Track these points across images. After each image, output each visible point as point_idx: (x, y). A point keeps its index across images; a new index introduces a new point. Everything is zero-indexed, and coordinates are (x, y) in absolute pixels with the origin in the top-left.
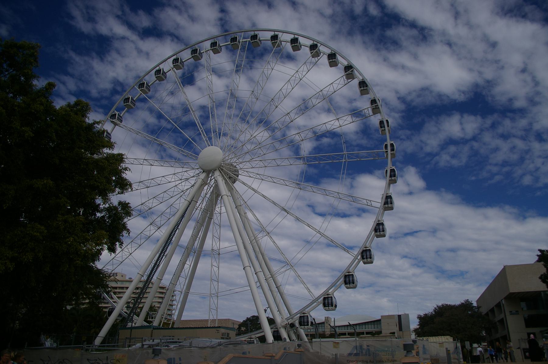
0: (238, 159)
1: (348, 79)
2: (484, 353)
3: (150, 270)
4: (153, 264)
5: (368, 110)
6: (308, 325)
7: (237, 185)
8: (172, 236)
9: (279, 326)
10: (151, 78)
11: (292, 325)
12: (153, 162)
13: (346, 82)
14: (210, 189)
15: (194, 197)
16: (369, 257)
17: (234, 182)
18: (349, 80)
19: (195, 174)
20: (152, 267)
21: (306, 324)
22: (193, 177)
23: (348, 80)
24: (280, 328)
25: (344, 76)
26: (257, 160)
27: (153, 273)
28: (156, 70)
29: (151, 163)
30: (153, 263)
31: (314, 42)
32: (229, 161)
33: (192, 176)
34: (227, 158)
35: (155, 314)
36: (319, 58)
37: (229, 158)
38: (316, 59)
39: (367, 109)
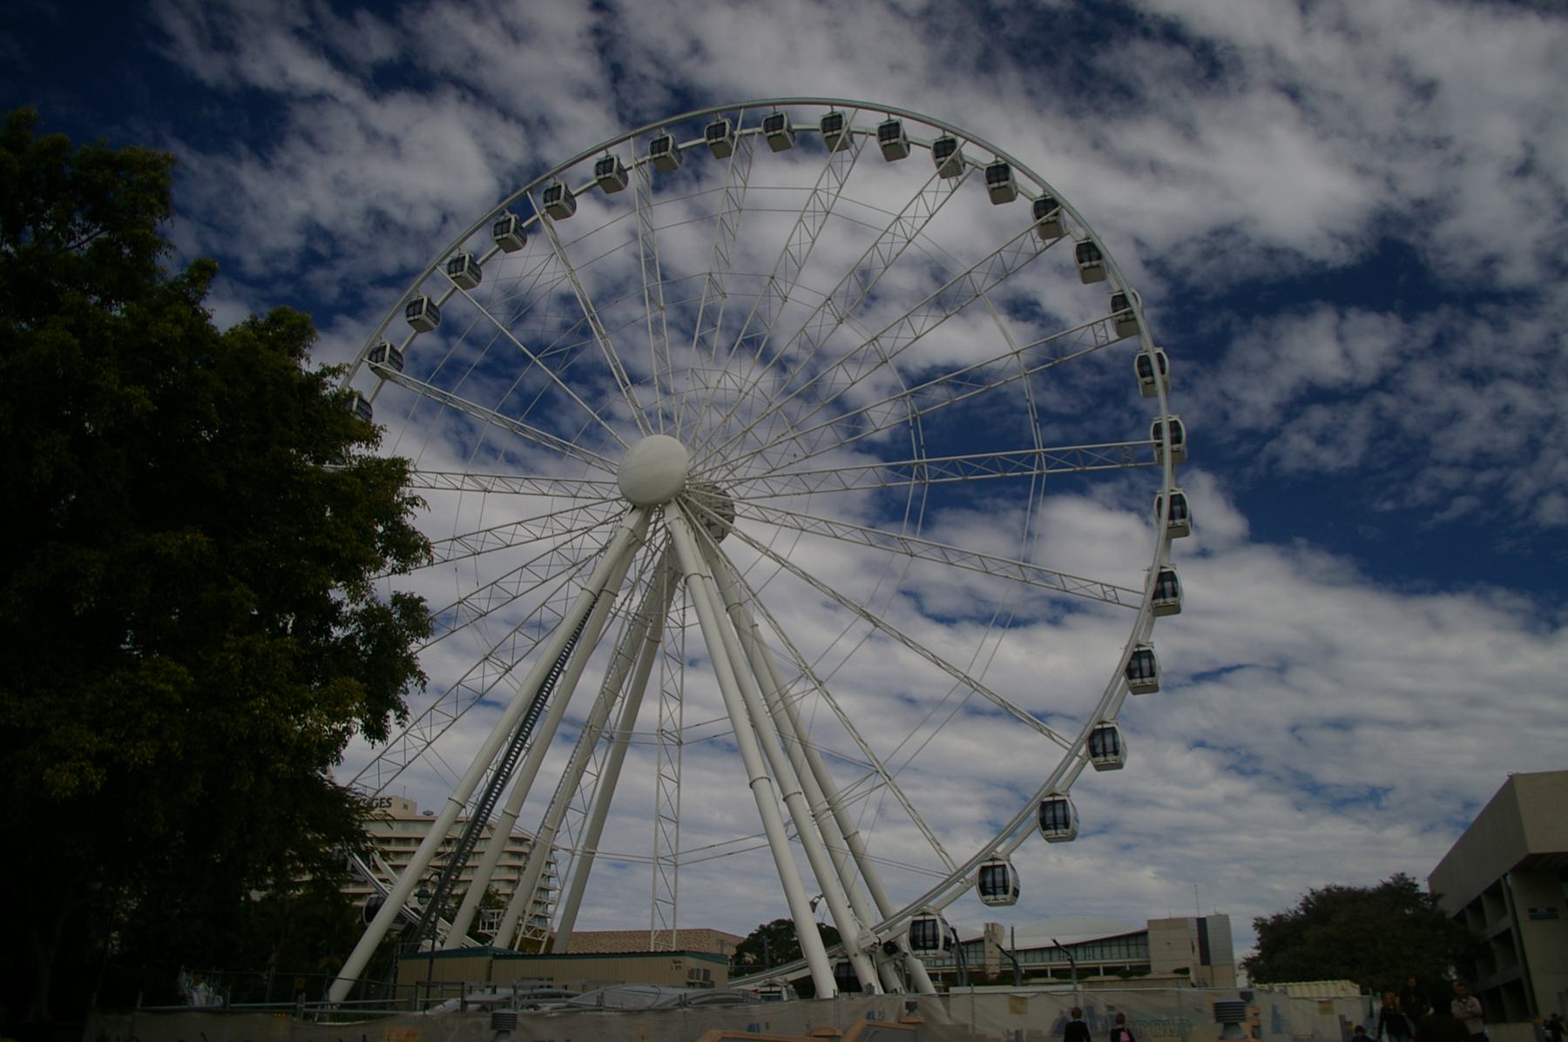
1: (1044, 237)
7: (730, 545)
14: (652, 559)
18: (1048, 242)
19: (609, 515)
24: (856, 955)
32: (707, 475)
33: (601, 520)
35: (498, 914)
36: (960, 178)
38: (953, 181)
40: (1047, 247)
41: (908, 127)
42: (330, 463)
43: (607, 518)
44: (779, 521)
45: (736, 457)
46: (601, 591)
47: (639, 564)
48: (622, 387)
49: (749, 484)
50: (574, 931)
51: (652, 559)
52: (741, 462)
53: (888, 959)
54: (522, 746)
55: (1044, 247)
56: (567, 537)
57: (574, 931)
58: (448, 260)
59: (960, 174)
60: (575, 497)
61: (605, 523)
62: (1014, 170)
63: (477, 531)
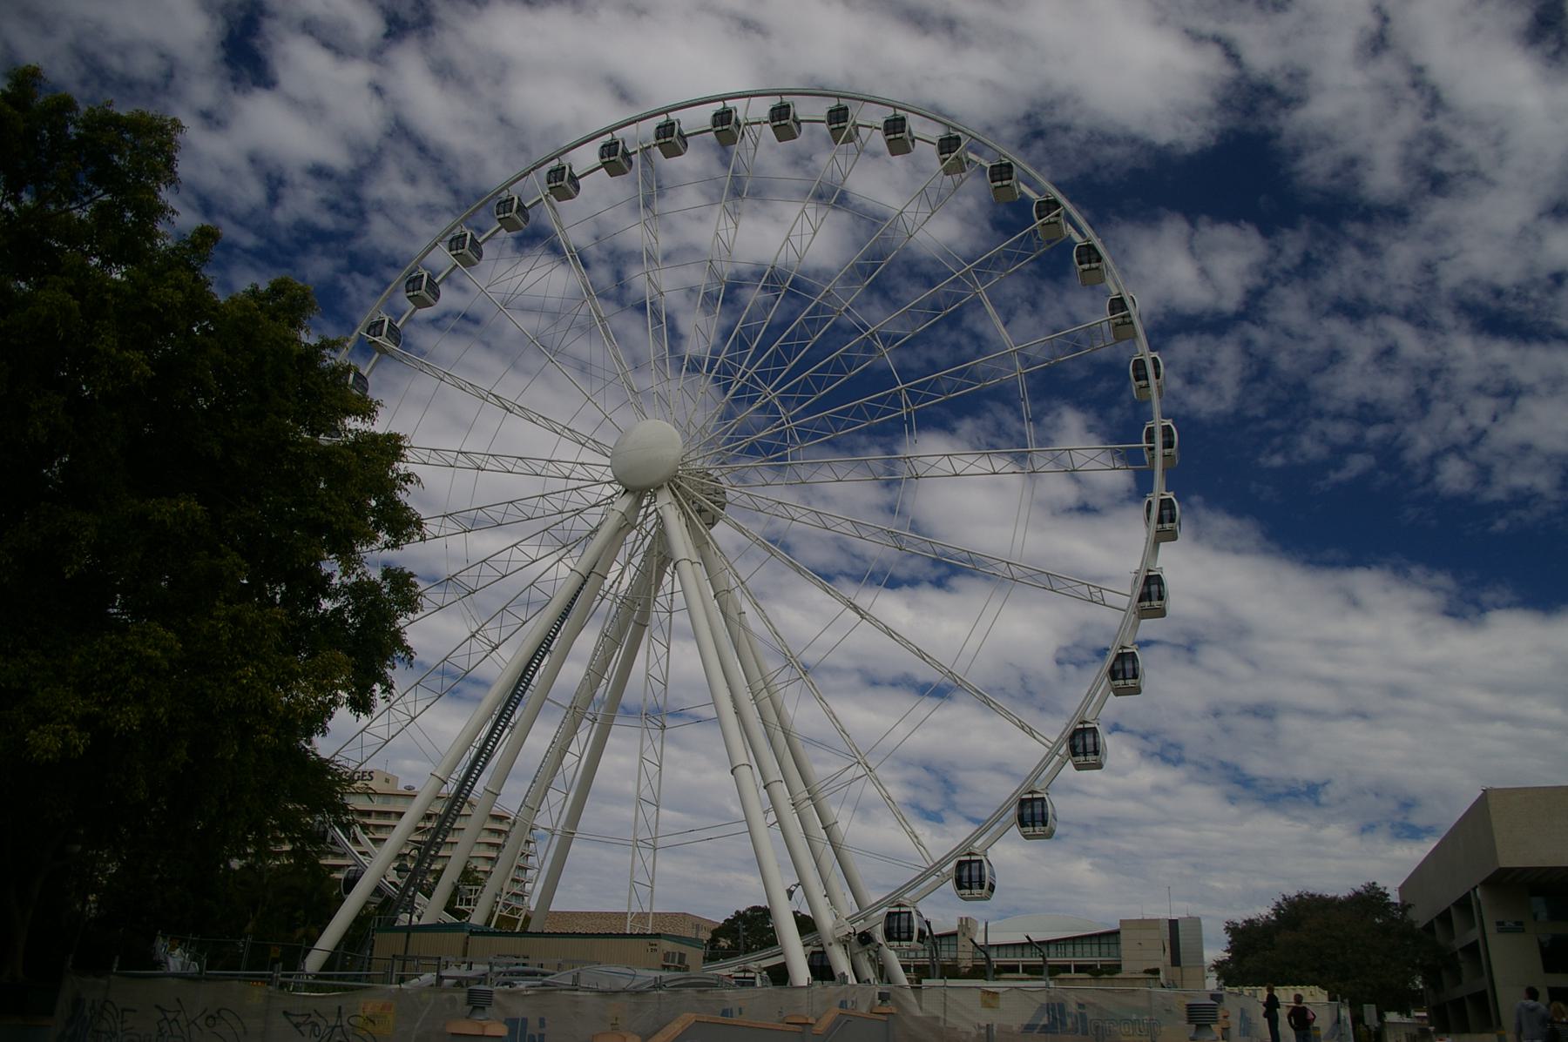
6: (910, 939)
21: (904, 935)
24: (830, 944)
29: (479, 462)
35: (476, 890)
53: (861, 949)
60: (567, 478)
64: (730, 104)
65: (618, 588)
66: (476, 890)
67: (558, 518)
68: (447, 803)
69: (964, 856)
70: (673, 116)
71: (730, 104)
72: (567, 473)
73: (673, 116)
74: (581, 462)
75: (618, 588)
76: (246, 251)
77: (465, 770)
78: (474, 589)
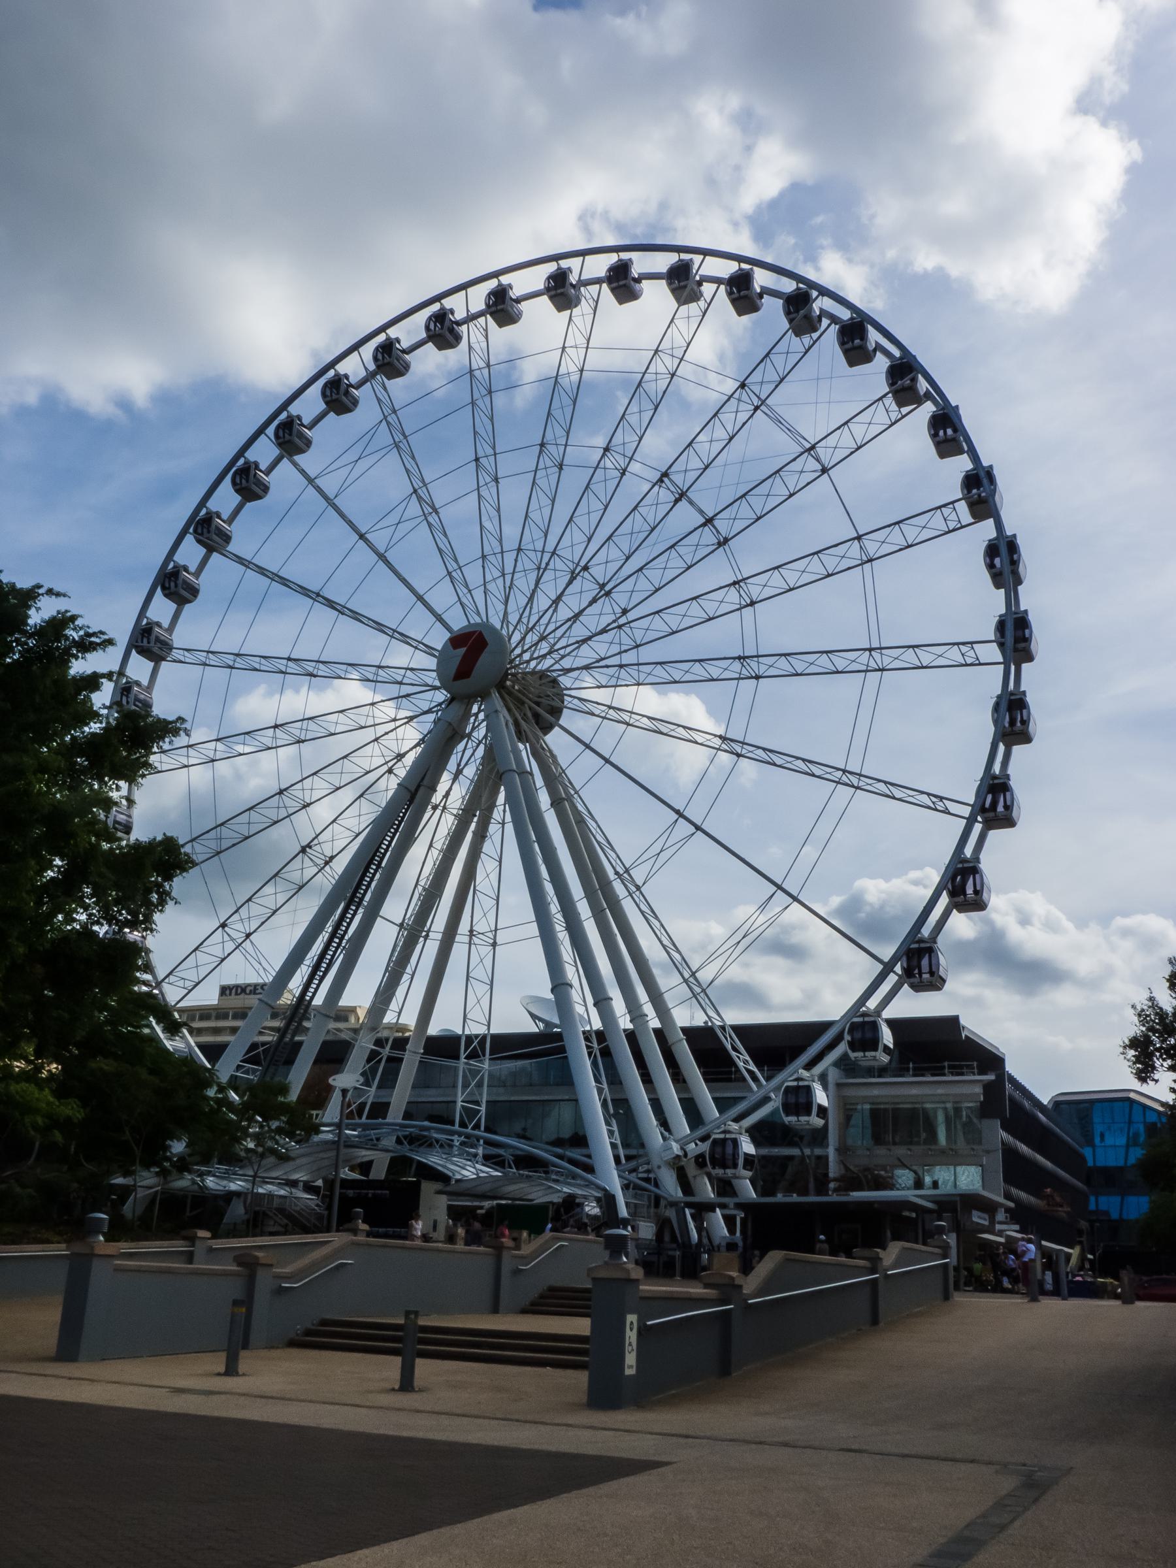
0: (556, 662)
1: (900, 404)
2: (184, 1182)
3: (318, 953)
4: (327, 934)
5: (954, 509)
6: (735, 1166)
7: (555, 740)
8: (364, 885)
9: (656, 1161)
10: (310, 405)
11: (700, 1160)
12: (301, 729)
13: (894, 416)
14: (473, 754)
15: (425, 775)
16: (927, 970)
17: (547, 728)
18: (905, 410)
19: (434, 704)
20: (304, 980)
21: (730, 1163)
22: (429, 711)
23: (902, 409)
24: (659, 1167)
25: (885, 396)
26: (609, 664)
27: (345, 924)
28: (325, 381)
29: (297, 732)
30: (327, 932)
31: (801, 285)
32: (533, 664)
33: (426, 709)
34: (526, 656)
35: (317, 1115)
36: (815, 335)
37: (536, 655)
38: (807, 340)
39: (951, 506)
40: (903, 417)
41: (762, 279)
42: (367, 1194)
43: (431, 706)
44: (603, 714)
45: (565, 644)
46: (419, 786)
47: (471, 725)
48: (353, 1121)
49: (575, 674)
50: (906, 985)
51: (473, 754)
52: (569, 649)
53: (699, 1172)
54: (339, 944)
55: (900, 416)
56: (392, 725)
57: (906, 985)
58: (276, 423)
59: (815, 330)
60: (401, 683)
61: (429, 711)
62: (870, 328)
63: (314, 836)
64: (564, 264)
65: (599, 592)
66: (317, 1115)
67: (392, 725)
68: (284, 1022)
69: (791, 1081)
70: (505, 279)
71: (564, 264)
72: (399, 679)
73: (505, 279)
74: (405, 694)
75: (599, 592)
76: (104, 678)
77: (301, 987)
78: (309, 802)
